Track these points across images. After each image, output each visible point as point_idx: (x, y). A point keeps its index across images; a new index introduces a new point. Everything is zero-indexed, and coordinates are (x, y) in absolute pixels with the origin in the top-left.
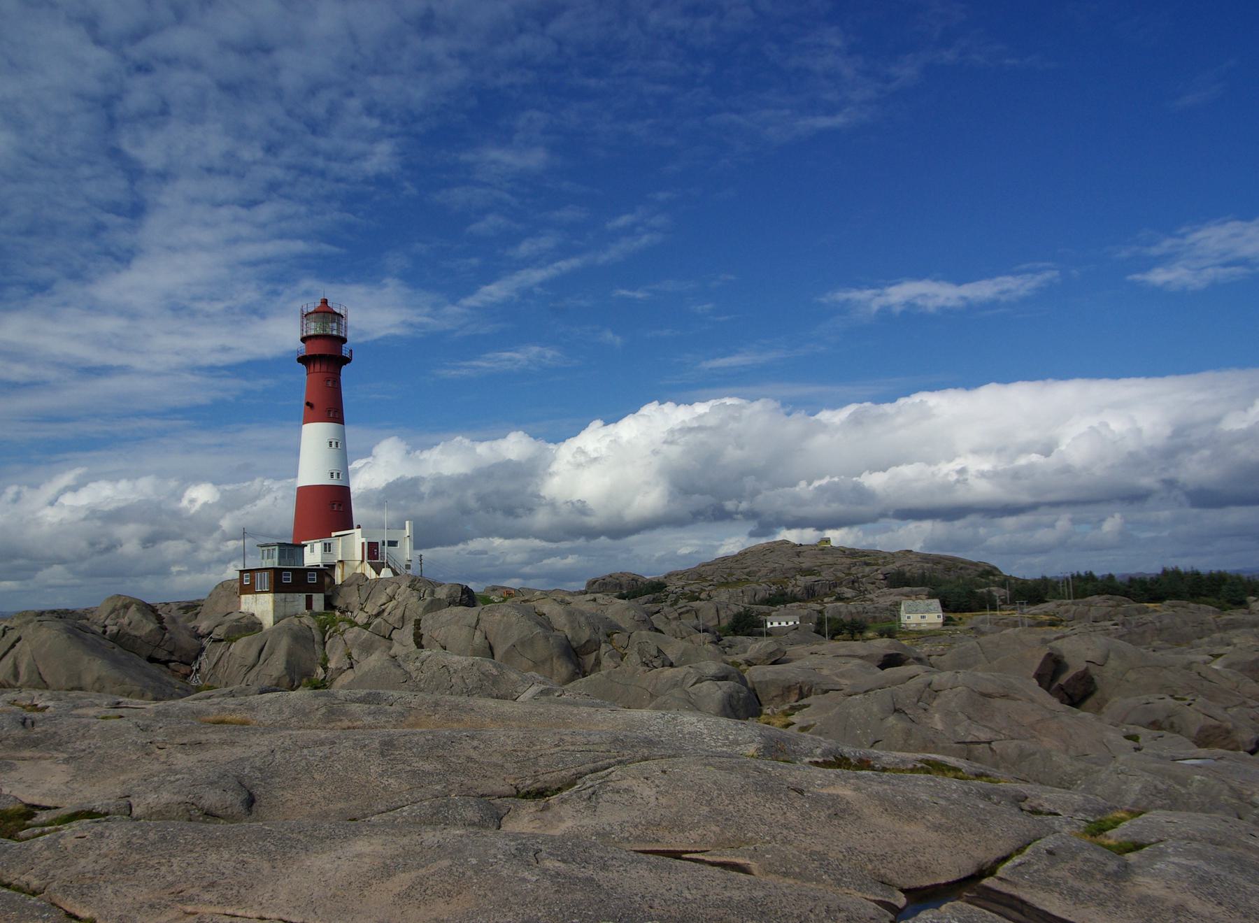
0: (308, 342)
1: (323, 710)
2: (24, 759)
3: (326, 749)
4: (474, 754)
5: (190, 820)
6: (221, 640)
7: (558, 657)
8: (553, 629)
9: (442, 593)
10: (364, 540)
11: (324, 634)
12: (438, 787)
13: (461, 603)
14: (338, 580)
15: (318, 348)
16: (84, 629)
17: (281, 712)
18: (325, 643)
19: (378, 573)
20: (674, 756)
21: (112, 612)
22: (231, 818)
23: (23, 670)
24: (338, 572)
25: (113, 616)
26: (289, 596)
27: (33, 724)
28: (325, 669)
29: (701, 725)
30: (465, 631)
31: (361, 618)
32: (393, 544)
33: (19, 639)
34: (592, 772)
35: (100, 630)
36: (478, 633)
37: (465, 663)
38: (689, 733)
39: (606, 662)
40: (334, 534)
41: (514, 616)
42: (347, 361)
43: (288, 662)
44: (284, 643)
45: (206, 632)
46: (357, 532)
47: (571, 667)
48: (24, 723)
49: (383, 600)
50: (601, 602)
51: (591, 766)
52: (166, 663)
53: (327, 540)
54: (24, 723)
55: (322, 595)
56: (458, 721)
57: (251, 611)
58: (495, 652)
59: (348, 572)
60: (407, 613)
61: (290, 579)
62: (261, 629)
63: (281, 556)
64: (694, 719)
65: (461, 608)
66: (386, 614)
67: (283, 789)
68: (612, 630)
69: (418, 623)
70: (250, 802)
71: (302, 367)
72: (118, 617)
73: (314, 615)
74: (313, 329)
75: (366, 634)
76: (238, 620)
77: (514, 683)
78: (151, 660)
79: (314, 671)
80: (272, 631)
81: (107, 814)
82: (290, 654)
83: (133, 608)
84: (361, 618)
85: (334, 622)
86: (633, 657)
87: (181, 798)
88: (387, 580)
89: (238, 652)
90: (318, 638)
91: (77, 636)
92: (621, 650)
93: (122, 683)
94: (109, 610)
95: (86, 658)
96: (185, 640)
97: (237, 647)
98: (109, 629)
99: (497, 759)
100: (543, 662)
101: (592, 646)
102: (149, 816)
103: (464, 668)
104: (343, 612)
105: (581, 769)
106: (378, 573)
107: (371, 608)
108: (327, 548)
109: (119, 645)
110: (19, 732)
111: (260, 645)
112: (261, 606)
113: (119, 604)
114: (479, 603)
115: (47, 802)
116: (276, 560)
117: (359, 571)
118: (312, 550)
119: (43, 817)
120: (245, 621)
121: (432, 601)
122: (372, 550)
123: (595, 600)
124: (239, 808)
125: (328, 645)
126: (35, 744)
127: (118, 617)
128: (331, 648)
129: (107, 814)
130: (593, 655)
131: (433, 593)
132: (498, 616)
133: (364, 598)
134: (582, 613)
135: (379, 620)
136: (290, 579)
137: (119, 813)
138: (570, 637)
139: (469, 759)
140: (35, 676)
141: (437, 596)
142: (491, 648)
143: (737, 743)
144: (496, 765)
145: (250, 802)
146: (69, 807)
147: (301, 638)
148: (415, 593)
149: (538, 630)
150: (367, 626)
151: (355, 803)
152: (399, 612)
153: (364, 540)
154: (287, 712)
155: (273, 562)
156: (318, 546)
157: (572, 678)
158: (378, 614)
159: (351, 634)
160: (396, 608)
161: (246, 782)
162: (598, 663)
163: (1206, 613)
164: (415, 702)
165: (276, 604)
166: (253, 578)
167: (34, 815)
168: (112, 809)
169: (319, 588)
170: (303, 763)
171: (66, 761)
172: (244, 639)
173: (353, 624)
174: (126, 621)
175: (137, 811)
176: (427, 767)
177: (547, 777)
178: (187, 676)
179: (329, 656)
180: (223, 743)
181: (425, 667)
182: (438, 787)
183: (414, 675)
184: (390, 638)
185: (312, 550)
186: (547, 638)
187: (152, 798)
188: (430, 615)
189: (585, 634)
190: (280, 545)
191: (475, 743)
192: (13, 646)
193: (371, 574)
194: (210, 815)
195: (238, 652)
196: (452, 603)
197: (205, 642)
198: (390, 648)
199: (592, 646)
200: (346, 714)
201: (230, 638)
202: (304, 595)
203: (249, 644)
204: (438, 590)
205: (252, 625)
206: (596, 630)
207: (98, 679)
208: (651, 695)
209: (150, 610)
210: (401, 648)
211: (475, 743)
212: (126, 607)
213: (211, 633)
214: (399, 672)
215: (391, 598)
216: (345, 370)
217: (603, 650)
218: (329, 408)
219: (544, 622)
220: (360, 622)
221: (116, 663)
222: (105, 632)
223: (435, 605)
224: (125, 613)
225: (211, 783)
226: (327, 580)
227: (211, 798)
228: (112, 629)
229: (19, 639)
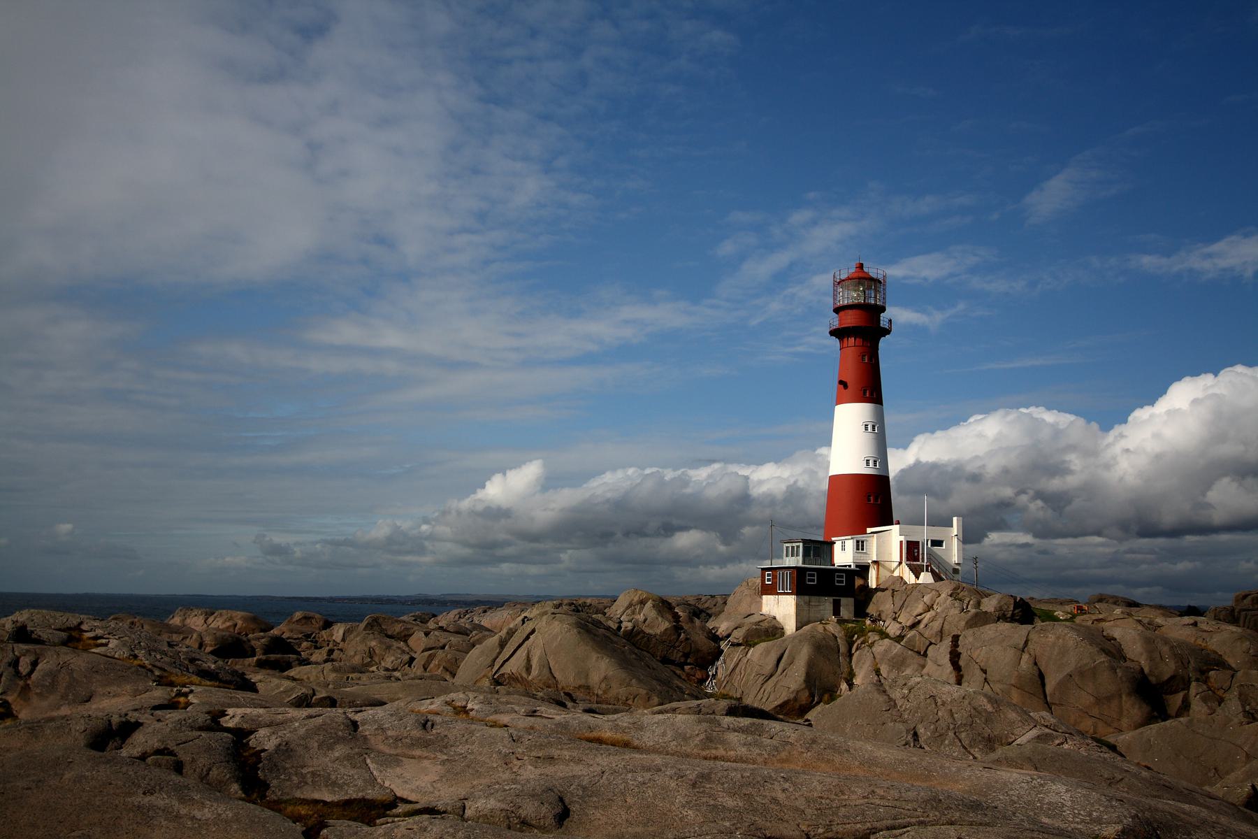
0: (842, 313)
1: (702, 736)
2: (413, 757)
3: (648, 775)
4: (781, 796)
5: (509, 828)
6: (739, 645)
7: (1129, 694)
8: (1125, 659)
9: (989, 605)
10: (902, 538)
11: (850, 645)
12: (727, 824)
13: (1012, 619)
14: (873, 583)
15: (851, 319)
16: (598, 624)
17: (664, 734)
18: (851, 656)
19: (917, 577)
20: (987, 824)
21: (627, 608)
22: (543, 829)
23: (534, 663)
24: (872, 573)
25: (629, 611)
26: (814, 598)
27: (433, 726)
28: (851, 685)
29: (1067, 797)
30: (1011, 653)
31: (893, 629)
32: (937, 543)
33: (533, 631)
34: (888, 829)
35: (614, 626)
36: (1025, 657)
37: (956, 695)
38: (1049, 803)
39: (1198, 707)
40: (869, 530)
41: (1071, 638)
42: (887, 332)
43: (808, 674)
44: (804, 654)
45: (725, 634)
46: (895, 529)
47: (1146, 708)
48: (424, 726)
49: (920, 608)
50: (1204, 627)
51: (890, 822)
52: (681, 666)
53: (860, 537)
54: (424, 726)
55: (851, 600)
56: (828, 761)
57: (773, 614)
58: (1047, 681)
59: (884, 574)
60: (946, 627)
61: (819, 583)
62: (783, 634)
63: (806, 554)
64: (1062, 789)
65: (1008, 625)
66: (922, 626)
67: (596, 808)
68: (1211, 662)
69: (956, 639)
70: (563, 816)
71: (835, 342)
72: (633, 613)
73: (841, 622)
74: (850, 296)
75: (897, 648)
76: (758, 623)
77: (1012, 723)
78: (665, 661)
79: (837, 686)
80: (793, 637)
81: (445, 812)
82: (811, 665)
83: (649, 604)
84: (893, 629)
85: (862, 632)
86: (1233, 705)
87: (503, 806)
88: (926, 586)
89: (755, 659)
90: (843, 649)
91: (588, 631)
92: (1220, 693)
93: (629, 685)
94: (626, 604)
95: (594, 656)
96: (700, 639)
97: (755, 653)
98: (623, 625)
99: (801, 804)
100: (1109, 699)
101: (1178, 683)
102: (476, 820)
103: (953, 700)
104: (874, 621)
105: (878, 825)
106: (917, 577)
107: (906, 619)
108: (860, 546)
109: (629, 646)
110: (417, 733)
111: (779, 653)
112: (782, 608)
113: (636, 599)
114: (1036, 619)
115: (412, 797)
116: (800, 558)
117: (896, 574)
118: (843, 548)
119: (401, 808)
120: (765, 625)
121: (976, 615)
122: (912, 550)
123: (1195, 624)
124: (550, 821)
125: (854, 658)
126: (426, 744)
127: (633, 613)
128: (858, 661)
129: (445, 812)
130: (1181, 695)
131: (978, 604)
132: (1051, 638)
133: (899, 604)
134: (1166, 641)
135: (913, 633)
136: (819, 583)
137: (454, 813)
138: (1146, 670)
139: (774, 800)
140: (546, 671)
141: (984, 608)
142: (1041, 676)
143: (1099, 821)
144: (797, 809)
145: (563, 816)
146: (424, 802)
147: (823, 649)
148: (957, 603)
149: (1102, 658)
150: (899, 639)
151: (651, 829)
152: (936, 625)
153: (902, 538)
154: (670, 734)
155: (795, 561)
156: (850, 544)
157: (1149, 720)
158: (913, 626)
159: (882, 646)
160: (933, 620)
161: (567, 801)
162: (1186, 706)
163: (596, 745)
164: (793, 737)
165: (798, 607)
166: (774, 577)
167: (396, 807)
168: (449, 809)
169: (848, 591)
170: (622, 787)
171: (443, 763)
172: (763, 645)
173: (884, 635)
174: (641, 617)
175: (468, 813)
176: (730, 803)
177: (840, 828)
178: (702, 681)
179: (856, 671)
180: (572, 760)
181: (912, 696)
182: (727, 824)
183: (899, 703)
184: (925, 655)
185: (843, 548)
186: (1113, 669)
187: (481, 804)
188: (970, 631)
189: (1168, 668)
190: (805, 541)
191: (787, 785)
192: (527, 638)
193: (910, 578)
194: (525, 824)
195: (755, 659)
196: (1002, 617)
197: (723, 645)
198: (923, 667)
199: (1178, 683)
200: (723, 742)
201: (748, 642)
202: (831, 599)
203: (767, 652)
204: (985, 600)
205: (772, 630)
206: (1182, 662)
207: (605, 678)
208: (1248, 756)
209: (664, 606)
210: (935, 667)
211: (787, 785)
212: (643, 602)
213: (729, 636)
214: (882, 698)
215: (930, 608)
216: (884, 343)
217: (1193, 691)
218: (867, 386)
219: (1114, 651)
220: (891, 634)
221: (624, 663)
222: (620, 628)
223: (980, 619)
224: (641, 609)
225: (533, 796)
226: (858, 582)
227: (529, 809)
228: (627, 625)
229: (533, 631)
